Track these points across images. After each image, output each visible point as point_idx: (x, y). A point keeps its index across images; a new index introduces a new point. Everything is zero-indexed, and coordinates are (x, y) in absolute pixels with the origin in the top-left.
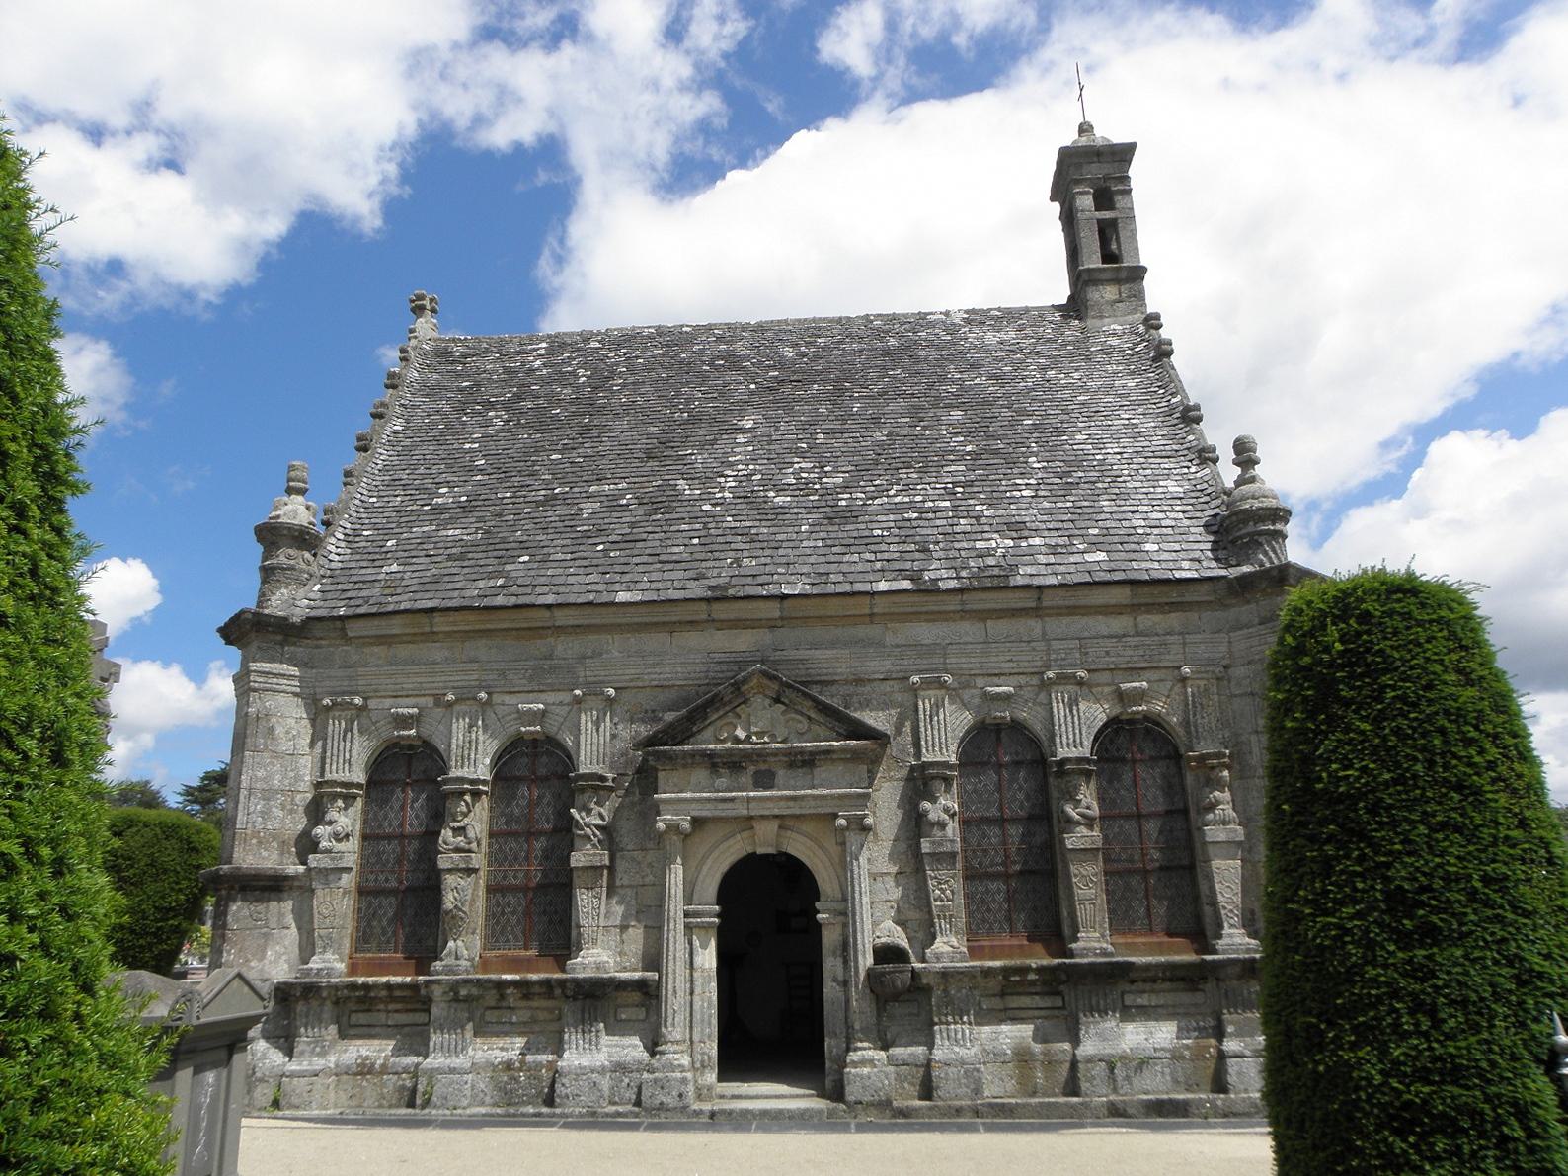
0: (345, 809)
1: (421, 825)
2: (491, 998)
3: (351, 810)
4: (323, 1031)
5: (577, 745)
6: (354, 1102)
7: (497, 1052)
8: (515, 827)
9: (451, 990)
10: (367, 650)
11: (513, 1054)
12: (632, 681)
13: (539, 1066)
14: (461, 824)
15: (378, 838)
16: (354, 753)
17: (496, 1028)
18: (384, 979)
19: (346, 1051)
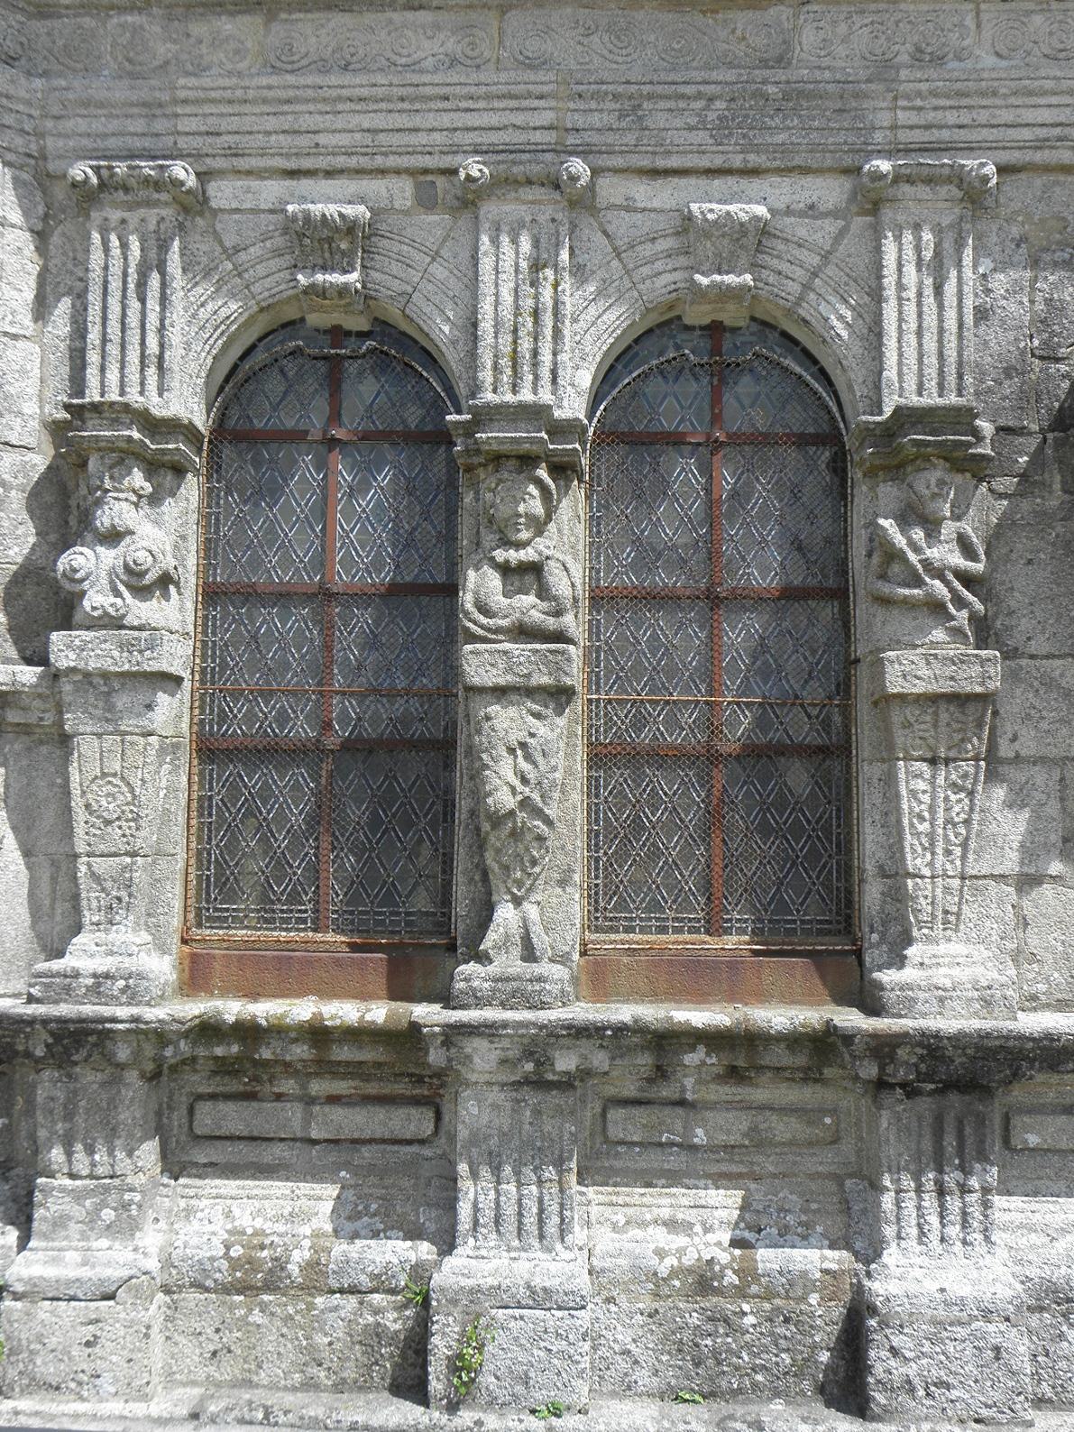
0: (155, 500)
1: (377, 565)
2: (627, 1078)
3: (170, 508)
4: (123, 1162)
5: (873, 334)
6: (228, 1370)
7: (660, 1236)
8: (663, 579)
9: (528, 1054)
10: (198, 29)
11: (713, 1245)
12: (1040, 144)
13: (797, 1284)
14: (527, 555)
15: (249, 595)
16: (175, 337)
17: (653, 1159)
18: (302, 1010)
19: (189, 1213)
